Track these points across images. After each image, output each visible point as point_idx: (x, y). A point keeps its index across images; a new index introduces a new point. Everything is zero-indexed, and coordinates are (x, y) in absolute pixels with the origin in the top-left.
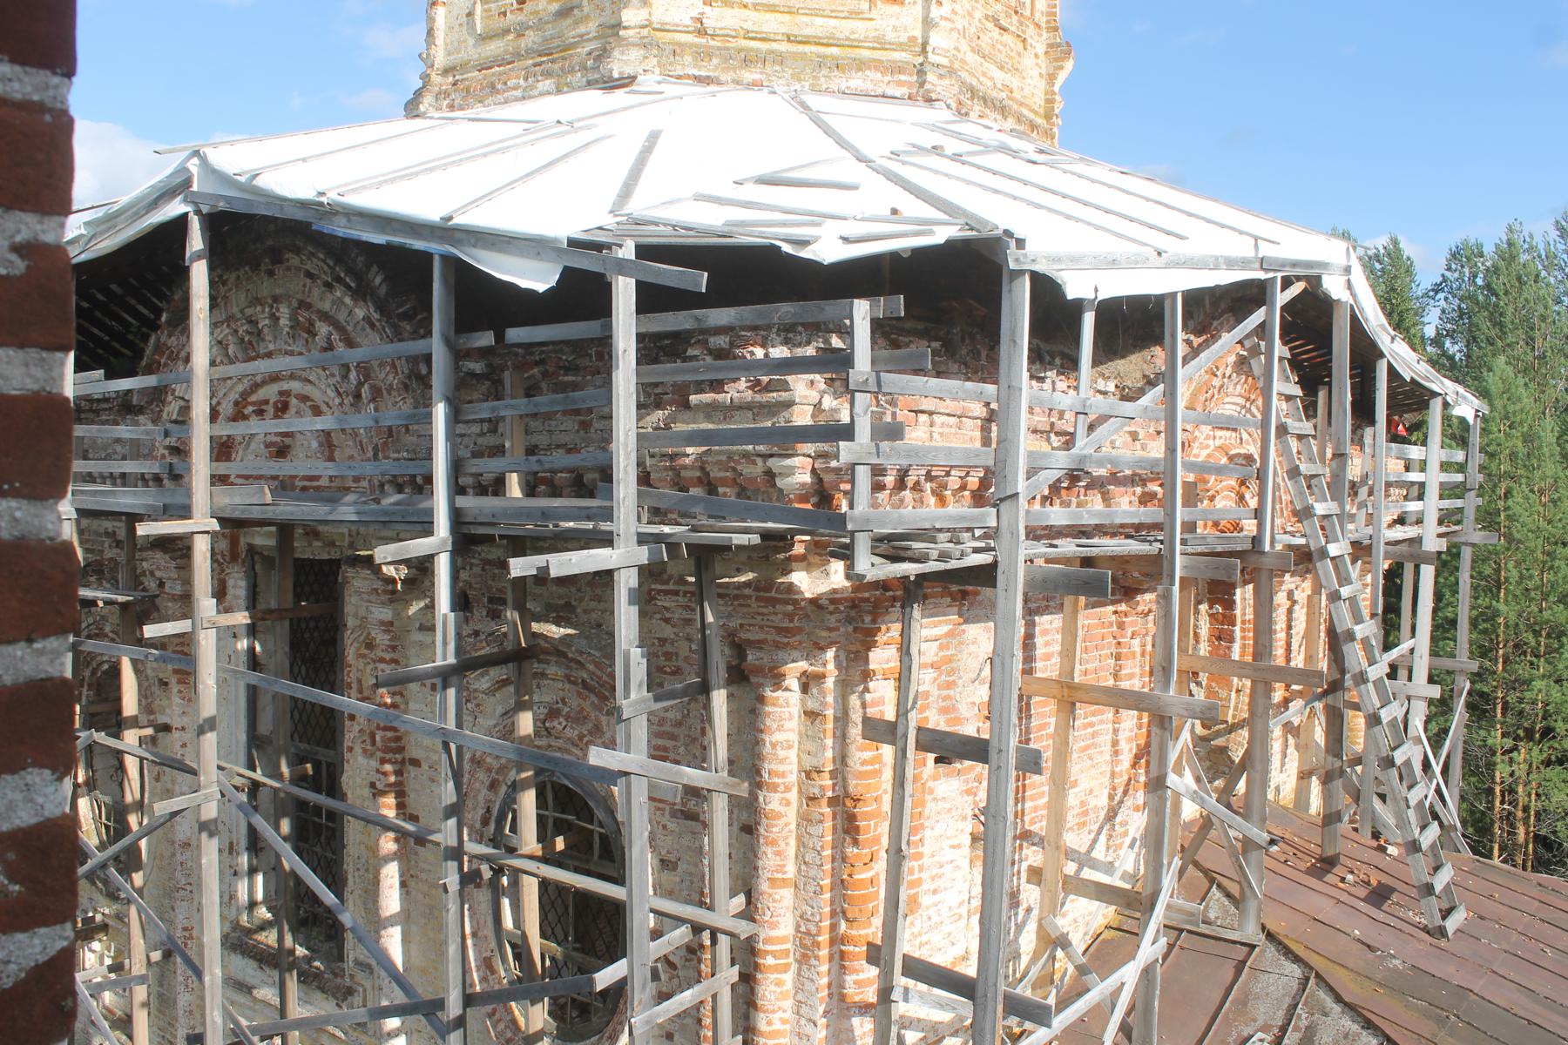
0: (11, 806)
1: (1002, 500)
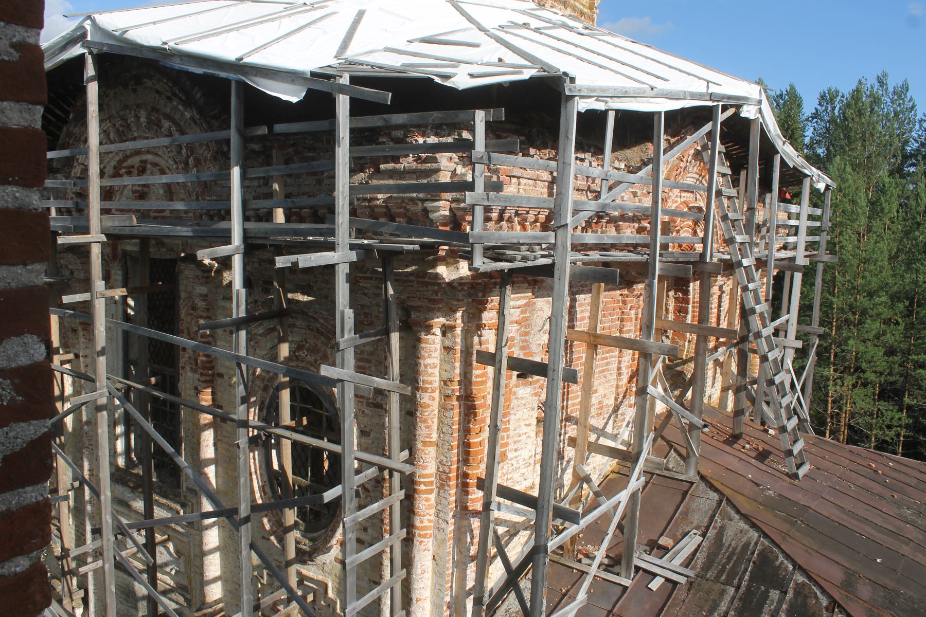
0: (16, 354)
1: (558, 228)
